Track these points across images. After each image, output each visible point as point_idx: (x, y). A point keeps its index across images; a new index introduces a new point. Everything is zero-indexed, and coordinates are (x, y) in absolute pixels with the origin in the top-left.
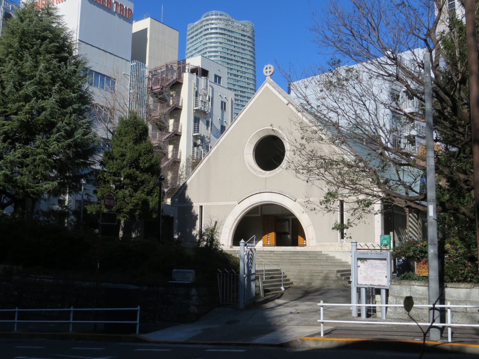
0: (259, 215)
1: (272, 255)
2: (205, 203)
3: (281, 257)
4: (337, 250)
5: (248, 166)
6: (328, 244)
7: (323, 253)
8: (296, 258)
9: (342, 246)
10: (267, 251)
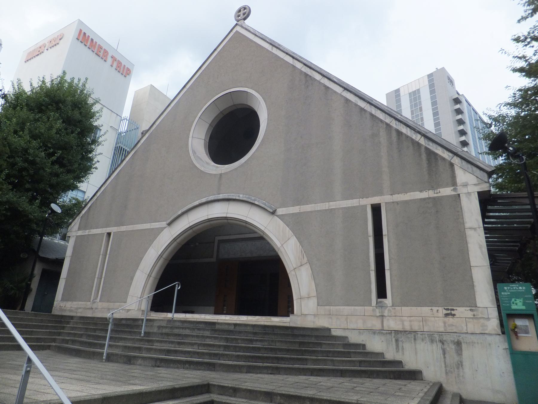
0: (214, 260)
5: (192, 157)
6: (347, 309)
7: (334, 333)
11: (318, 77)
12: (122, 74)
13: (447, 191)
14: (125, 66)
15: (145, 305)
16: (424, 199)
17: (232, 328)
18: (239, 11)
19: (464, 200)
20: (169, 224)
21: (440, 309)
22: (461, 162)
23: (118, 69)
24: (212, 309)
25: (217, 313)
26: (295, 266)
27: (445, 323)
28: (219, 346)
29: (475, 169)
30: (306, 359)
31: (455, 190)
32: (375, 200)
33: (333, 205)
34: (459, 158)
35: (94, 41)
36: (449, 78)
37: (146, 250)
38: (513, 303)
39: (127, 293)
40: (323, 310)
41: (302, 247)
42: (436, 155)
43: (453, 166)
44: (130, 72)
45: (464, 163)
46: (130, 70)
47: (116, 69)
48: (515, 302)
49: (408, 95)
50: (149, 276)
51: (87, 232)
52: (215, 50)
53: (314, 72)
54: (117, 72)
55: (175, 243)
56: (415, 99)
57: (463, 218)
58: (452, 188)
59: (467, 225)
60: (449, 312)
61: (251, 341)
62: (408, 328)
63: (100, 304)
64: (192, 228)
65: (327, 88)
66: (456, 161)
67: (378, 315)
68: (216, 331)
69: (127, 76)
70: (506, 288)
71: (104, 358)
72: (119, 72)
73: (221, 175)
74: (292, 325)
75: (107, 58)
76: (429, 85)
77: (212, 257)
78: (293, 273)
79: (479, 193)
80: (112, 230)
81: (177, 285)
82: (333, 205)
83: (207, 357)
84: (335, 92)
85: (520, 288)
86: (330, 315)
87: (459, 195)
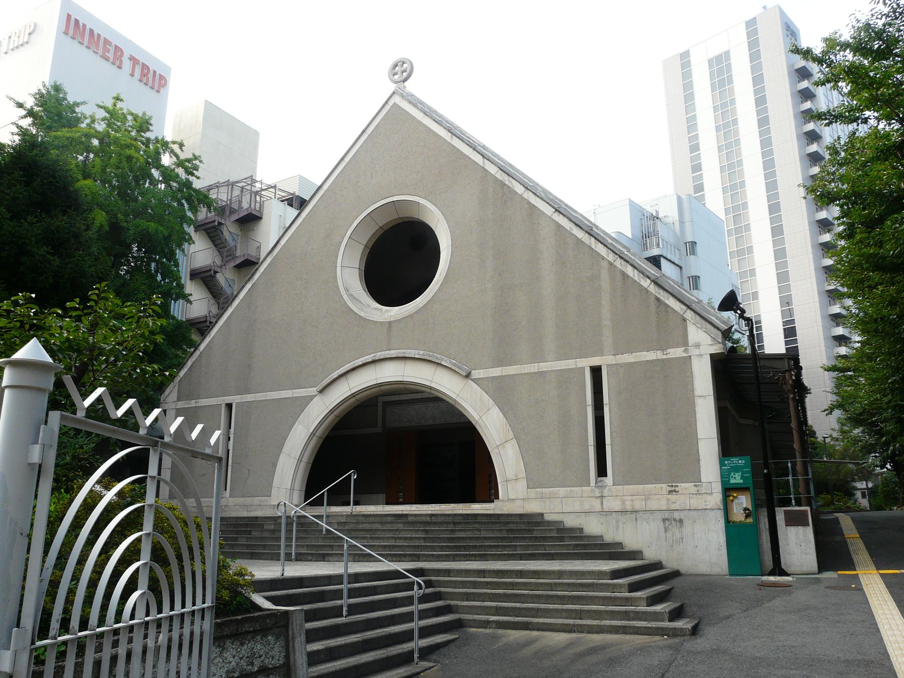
0: (379, 430)
1: (401, 526)
2: (239, 396)
3: (426, 531)
4: (587, 507)
5: (345, 297)
6: (562, 491)
7: (548, 517)
8: (469, 534)
9: (602, 497)
10: (387, 515)
11: (519, 189)
12: (152, 88)
13: (676, 352)
14: (155, 72)
15: (297, 496)
16: (652, 361)
17: (428, 519)
18: (396, 65)
19: (696, 363)
20: (321, 391)
21: (664, 485)
23: (145, 80)
24: (382, 497)
25: (388, 503)
26: (498, 443)
27: (668, 500)
28: (419, 538)
29: (709, 326)
30: (516, 546)
31: (686, 351)
32: (595, 361)
33: (544, 366)
34: (692, 313)
35: (95, 33)
36: (789, 27)
37: (291, 427)
38: (732, 477)
39: (270, 484)
40: (533, 493)
41: (506, 419)
42: (667, 306)
43: (686, 321)
44: (166, 81)
45: (698, 318)
46: (165, 78)
47: (141, 81)
48: (734, 476)
49: (707, 61)
50: (300, 460)
52: (364, 131)
53: (514, 181)
54: (142, 85)
55: (332, 416)
56: (720, 72)
57: (693, 385)
58: (683, 349)
59: (697, 393)
60: (673, 488)
61: (453, 531)
62: (629, 508)
63: (231, 500)
64: (354, 396)
65: (532, 207)
66: (689, 315)
67: (598, 495)
69: (162, 90)
70: (726, 462)
71: (293, 557)
72: (146, 84)
73: (390, 323)
75: (121, 62)
76: (748, 42)
78: (496, 450)
79: (712, 356)
80: (235, 399)
81: (352, 474)
82: (544, 366)
83: (408, 549)
84: (543, 213)
85: (740, 462)
86: (542, 498)
87: (690, 356)
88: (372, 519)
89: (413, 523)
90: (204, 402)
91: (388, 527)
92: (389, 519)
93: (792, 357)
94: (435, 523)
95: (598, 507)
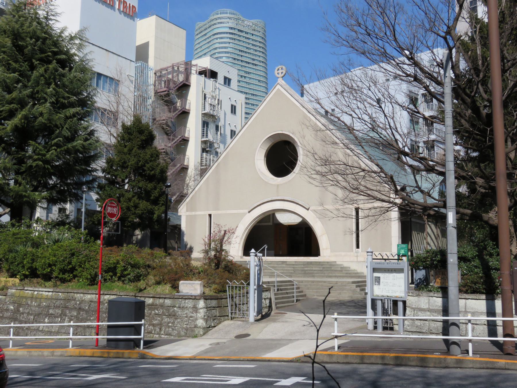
0: (271, 224)
1: (284, 266)
3: (293, 267)
5: (259, 173)
6: (343, 253)
7: (337, 263)
17: (294, 263)
20: (249, 212)
22: (190, 108)
51: (193, 213)
68: (287, 264)
73: (278, 185)
74: (320, 261)
77: (270, 222)
88: (273, 263)
89: (289, 265)
90: (198, 213)
91: (280, 266)
92: (280, 263)
93: (405, 157)
94: (297, 265)
95: (356, 260)
